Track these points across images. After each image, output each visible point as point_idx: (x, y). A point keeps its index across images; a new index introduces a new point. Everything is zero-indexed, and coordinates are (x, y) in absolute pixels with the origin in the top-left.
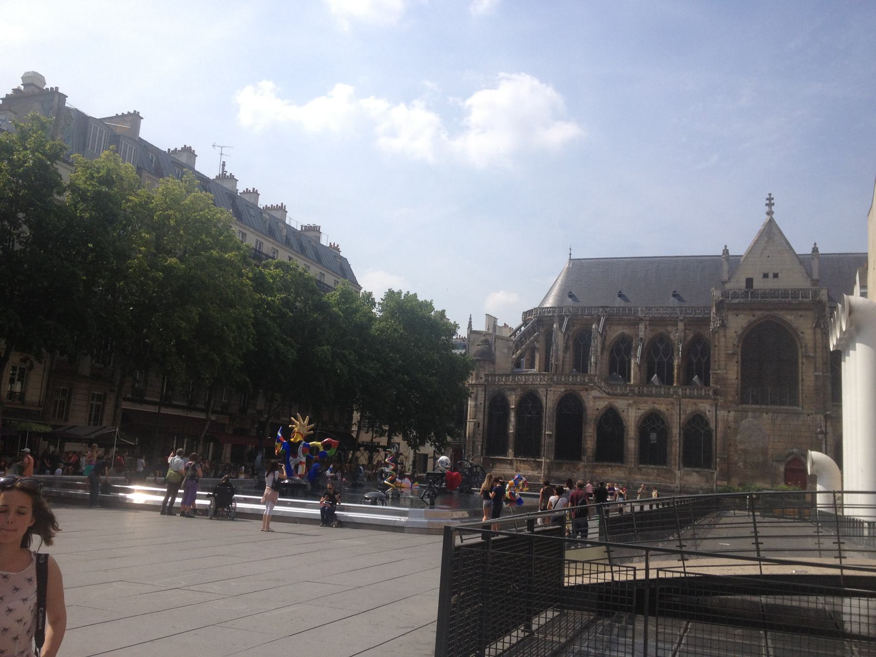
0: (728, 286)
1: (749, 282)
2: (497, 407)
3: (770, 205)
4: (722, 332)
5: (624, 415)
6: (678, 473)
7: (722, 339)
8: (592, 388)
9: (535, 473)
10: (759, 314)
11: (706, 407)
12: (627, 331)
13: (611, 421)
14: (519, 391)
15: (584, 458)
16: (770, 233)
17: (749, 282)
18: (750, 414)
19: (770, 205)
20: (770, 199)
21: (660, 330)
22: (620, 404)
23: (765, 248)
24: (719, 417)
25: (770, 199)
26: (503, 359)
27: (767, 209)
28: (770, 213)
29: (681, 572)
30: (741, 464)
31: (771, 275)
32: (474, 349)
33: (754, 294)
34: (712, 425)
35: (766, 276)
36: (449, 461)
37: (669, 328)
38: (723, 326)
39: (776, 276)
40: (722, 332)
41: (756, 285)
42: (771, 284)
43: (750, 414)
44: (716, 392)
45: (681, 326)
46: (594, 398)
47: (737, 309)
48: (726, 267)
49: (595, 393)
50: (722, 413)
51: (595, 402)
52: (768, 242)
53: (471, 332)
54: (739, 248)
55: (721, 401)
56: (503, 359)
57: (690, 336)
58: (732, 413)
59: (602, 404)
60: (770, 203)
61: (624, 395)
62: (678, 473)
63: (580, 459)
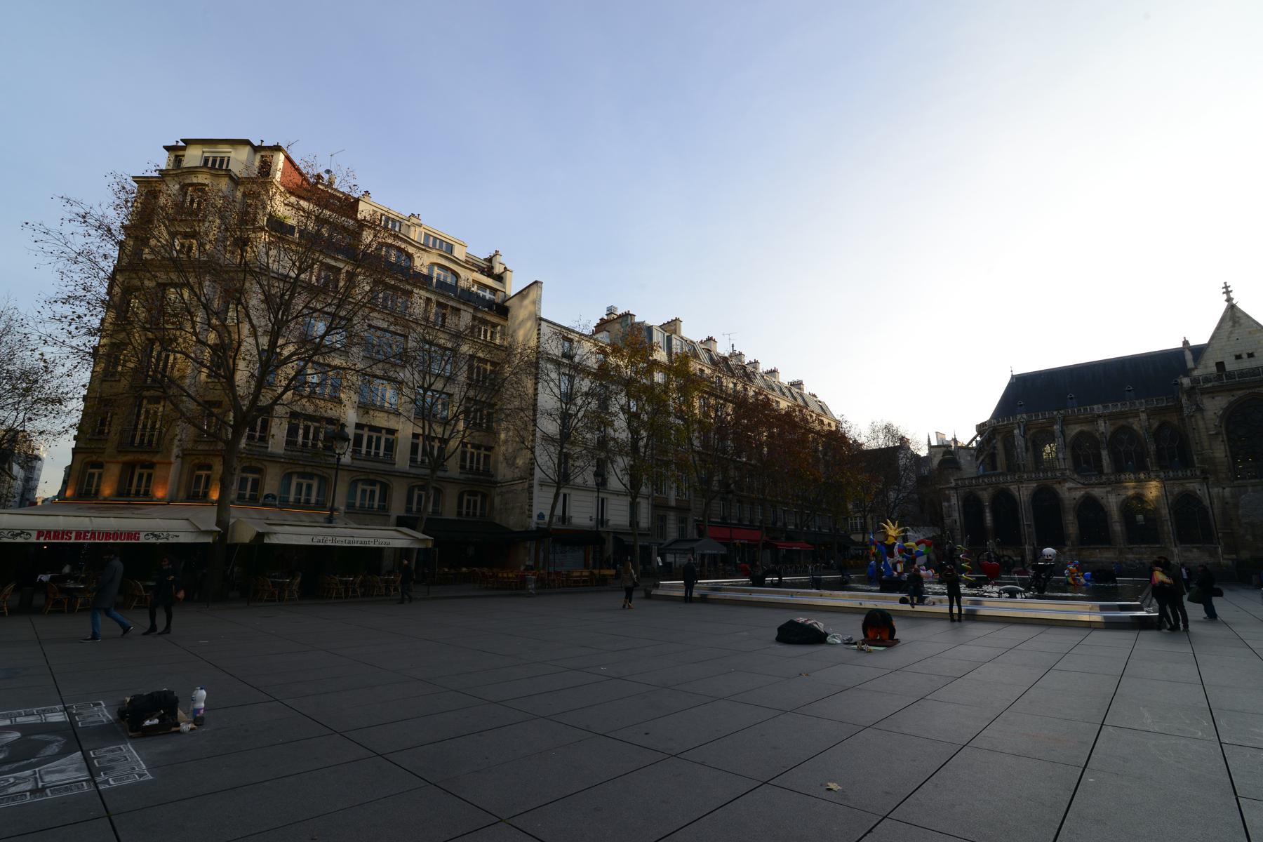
0: (1196, 373)
1: (1220, 365)
2: (971, 506)
3: (1228, 292)
4: (1199, 416)
5: (1103, 501)
6: (1176, 551)
7: (1201, 423)
8: (1065, 480)
9: (50, 483)
10: (1240, 393)
11: (1196, 487)
12: (1085, 428)
13: (1090, 507)
14: (990, 490)
15: (1069, 543)
16: (1233, 316)
17: (1220, 365)
18: (1250, 489)
19: (1228, 292)
20: (1226, 287)
21: (1122, 422)
22: (1097, 492)
23: (1231, 333)
24: (1212, 494)
25: (1226, 287)
26: (969, 468)
27: (1225, 297)
28: (1229, 300)
29: (48, 773)
30: (1249, 537)
31: (1245, 356)
32: (936, 462)
33: (1231, 375)
34: (1207, 502)
35: (1238, 357)
36: (533, 523)
37: (1131, 420)
38: (1200, 409)
39: (1251, 355)
40: (1199, 416)
41: (1228, 368)
42: (1246, 364)
43: (1250, 489)
44: (1203, 471)
45: (1143, 416)
46: (1070, 489)
47: (1212, 392)
48: (1189, 356)
49: (1068, 485)
50: (1215, 491)
51: (1071, 492)
52: (1233, 326)
53: (930, 447)
54: (1200, 337)
55: (1212, 479)
56: (969, 468)
57: (1156, 424)
58: (1228, 490)
59: (1078, 494)
60: (1227, 290)
61: (1100, 484)
62: (1176, 551)
63: (1065, 545)
